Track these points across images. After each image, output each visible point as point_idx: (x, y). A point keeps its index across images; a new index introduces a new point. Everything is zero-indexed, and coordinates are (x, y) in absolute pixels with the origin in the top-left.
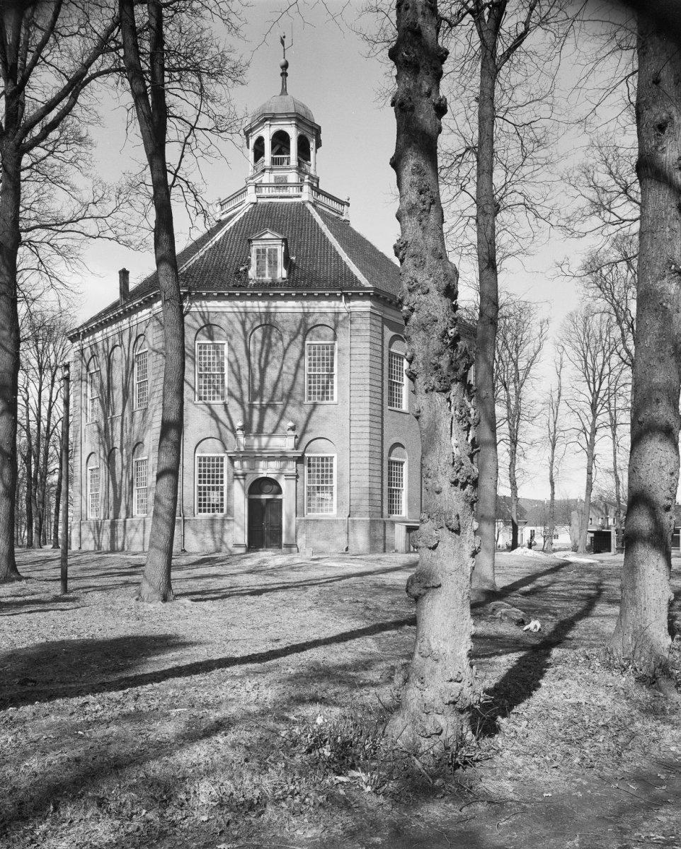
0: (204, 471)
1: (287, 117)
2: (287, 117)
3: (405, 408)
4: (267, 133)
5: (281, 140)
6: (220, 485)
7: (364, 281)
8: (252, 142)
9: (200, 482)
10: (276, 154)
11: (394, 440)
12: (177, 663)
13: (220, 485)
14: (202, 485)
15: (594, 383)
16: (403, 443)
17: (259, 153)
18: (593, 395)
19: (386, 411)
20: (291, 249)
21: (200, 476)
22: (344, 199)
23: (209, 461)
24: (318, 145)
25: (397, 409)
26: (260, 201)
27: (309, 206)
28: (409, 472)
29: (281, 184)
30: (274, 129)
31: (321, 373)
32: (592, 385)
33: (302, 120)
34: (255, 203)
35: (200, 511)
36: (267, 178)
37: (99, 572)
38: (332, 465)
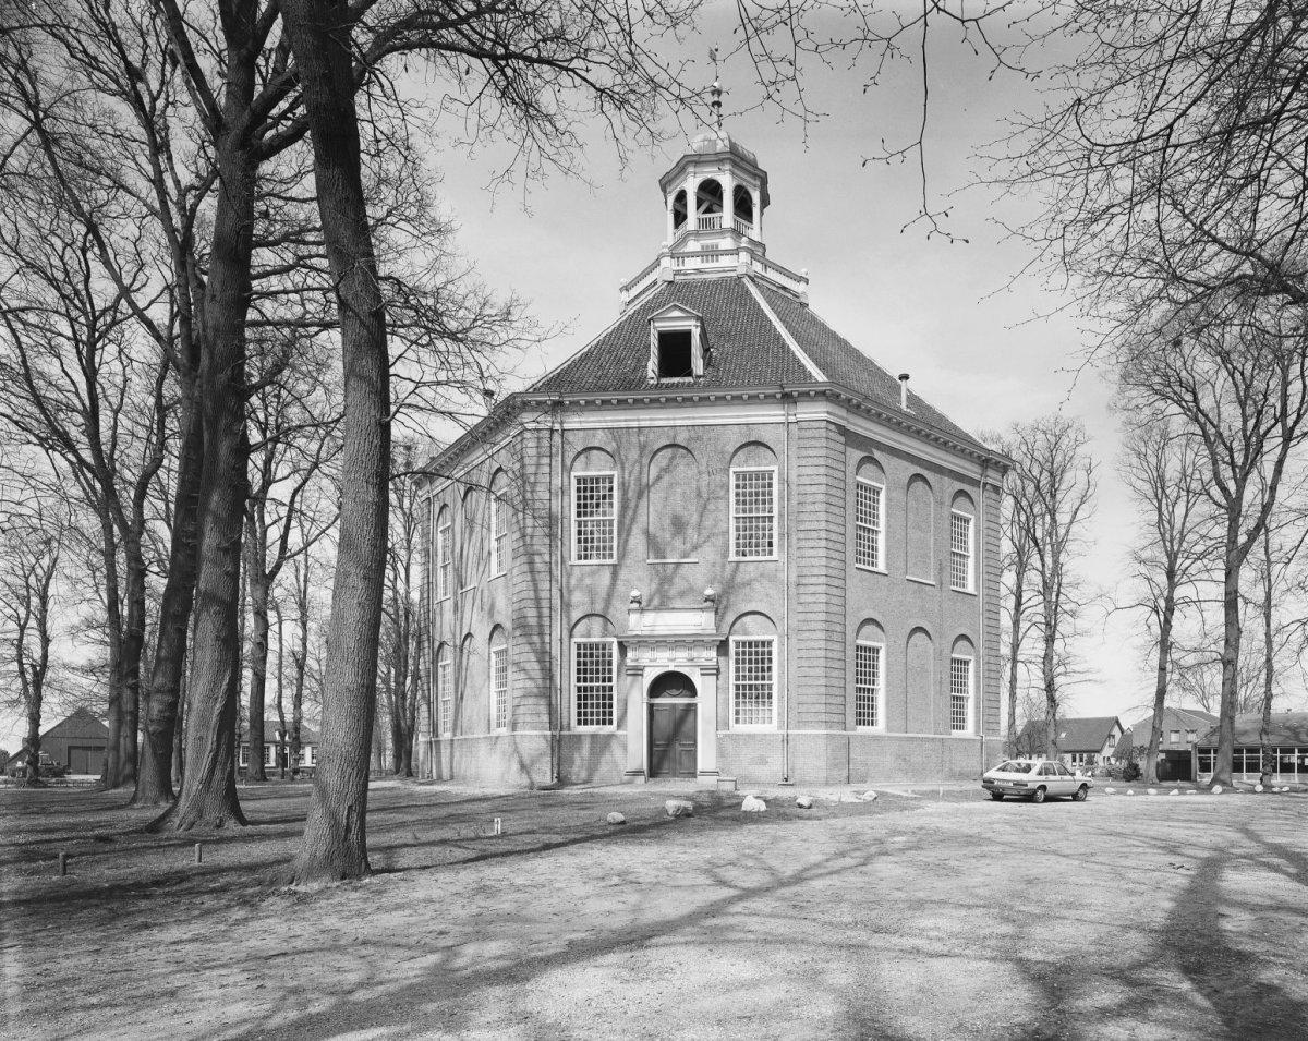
0: (585, 656)
1: (718, 160)
2: (718, 160)
3: (881, 567)
4: (691, 185)
5: (710, 190)
6: (607, 684)
7: (819, 375)
8: (671, 199)
9: (579, 680)
10: (706, 212)
11: (866, 614)
12: (101, 396)
13: (607, 684)
14: (582, 684)
15: (1171, 542)
16: (879, 618)
17: (680, 218)
18: (1169, 556)
19: (851, 571)
20: (708, 329)
21: (579, 671)
22: (802, 272)
23: (597, 649)
24: (765, 202)
25: (870, 568)
26: (677, 277)
27: (746, 280)
28: (888, 663)
29: (712, 253)
30: (699, 180)
31: (754, 514)
32: (1168, 544)
33: (737, 158)
34: (671, 282)
35: (579, 723)
36: (693, 246)
37: (460, 854)
38: (770, 653)
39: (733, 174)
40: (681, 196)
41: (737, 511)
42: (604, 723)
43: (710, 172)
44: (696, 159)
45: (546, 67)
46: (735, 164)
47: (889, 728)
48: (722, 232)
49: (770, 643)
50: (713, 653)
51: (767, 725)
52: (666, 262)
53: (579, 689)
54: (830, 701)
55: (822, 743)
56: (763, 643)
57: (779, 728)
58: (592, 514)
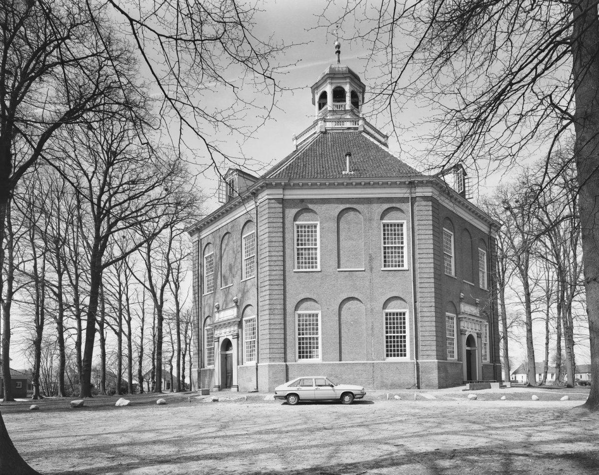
4: (329, 89)
14: (403, 334)
33: (353, 77)
39: (351, 85)
40: (324, 95)
41: (316, 254)
42: (401, 356)
43: (338, 83)
44: (315, 86)
45: (107, 137)
46: (352, 80)
47: (323, 360)
48: (345, 111)
49: (404, 314)
50: (236, 328)
51: (403, 357)
52: (320, 123)
53: (405, 332)
54: (273, 347)
55: (267, 369)
56: (400, 314)
57: (411, 358)
58: (305, 244)
